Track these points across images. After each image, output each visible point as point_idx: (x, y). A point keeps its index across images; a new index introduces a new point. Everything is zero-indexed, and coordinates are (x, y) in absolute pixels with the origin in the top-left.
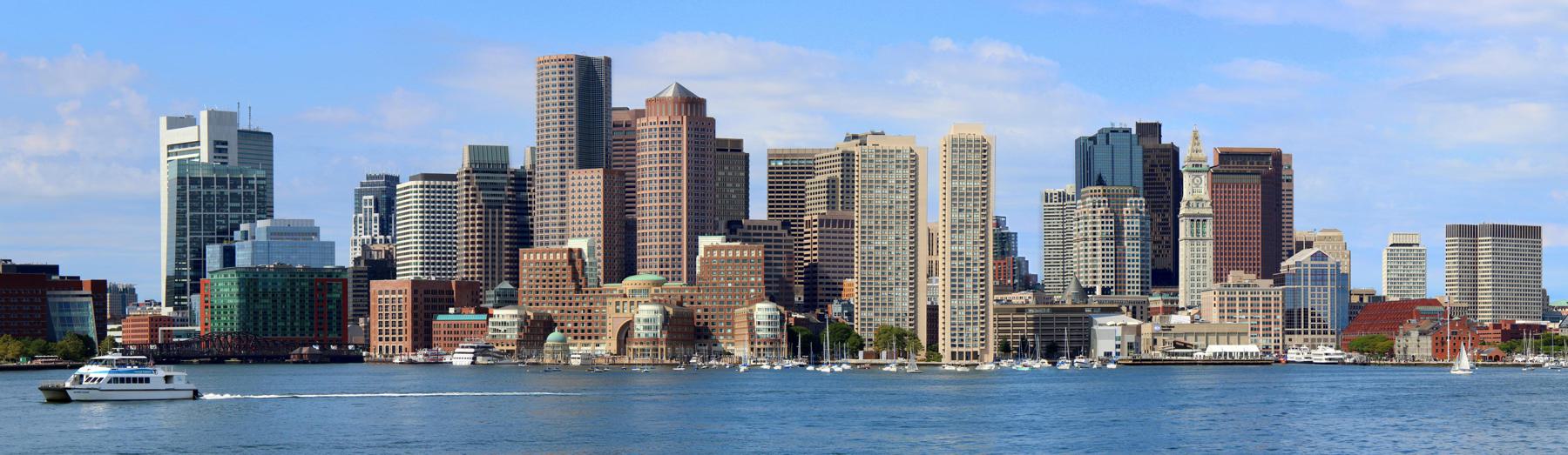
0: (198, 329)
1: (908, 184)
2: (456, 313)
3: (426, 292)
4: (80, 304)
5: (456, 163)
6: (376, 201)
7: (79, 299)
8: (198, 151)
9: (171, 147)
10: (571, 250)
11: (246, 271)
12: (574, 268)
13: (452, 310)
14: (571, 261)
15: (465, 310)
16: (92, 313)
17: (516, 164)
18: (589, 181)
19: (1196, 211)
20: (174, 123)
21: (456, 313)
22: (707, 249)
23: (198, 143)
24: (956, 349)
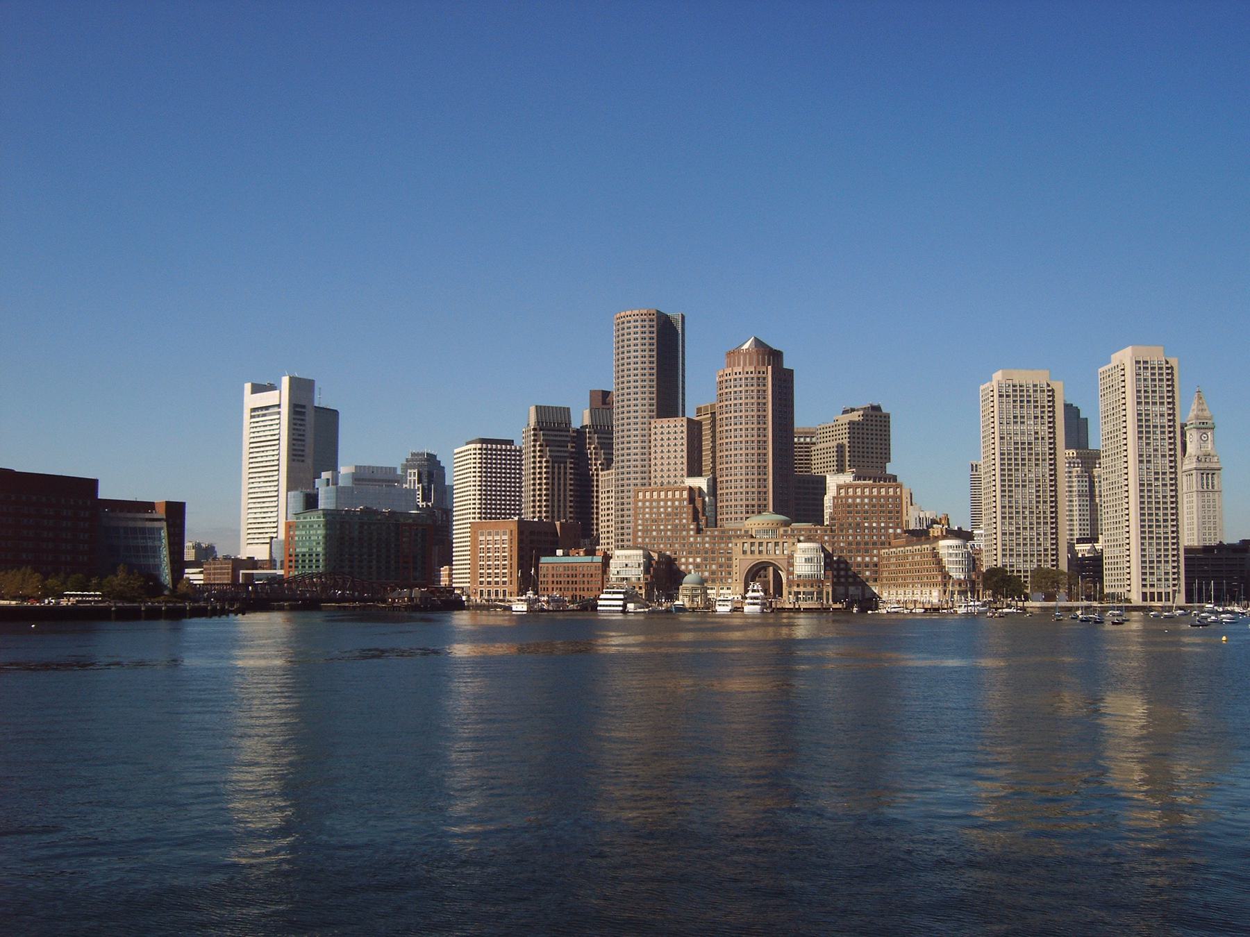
0: (280, 572)
1: (1046, 420)
2: (564, 555)
3: (532, 533)
4: (152, 530)
5: (519, 428)
6: (420, 474)
7: (149, 524)
8: (279, 413)
9: (254, 410)
10: (691, 489)
11: (327, 513)
12: (695, 509)
13: (559, 552)
14: (692, 500)
15: (572, 551)
16: (165, 542)
17: (576, 425)
18: (672, 430)
19: (1206, 465)
20: (257, 389)
21: (564, 555)
22: (839, 487)
23: (279, 406)
24: (1148, 590)
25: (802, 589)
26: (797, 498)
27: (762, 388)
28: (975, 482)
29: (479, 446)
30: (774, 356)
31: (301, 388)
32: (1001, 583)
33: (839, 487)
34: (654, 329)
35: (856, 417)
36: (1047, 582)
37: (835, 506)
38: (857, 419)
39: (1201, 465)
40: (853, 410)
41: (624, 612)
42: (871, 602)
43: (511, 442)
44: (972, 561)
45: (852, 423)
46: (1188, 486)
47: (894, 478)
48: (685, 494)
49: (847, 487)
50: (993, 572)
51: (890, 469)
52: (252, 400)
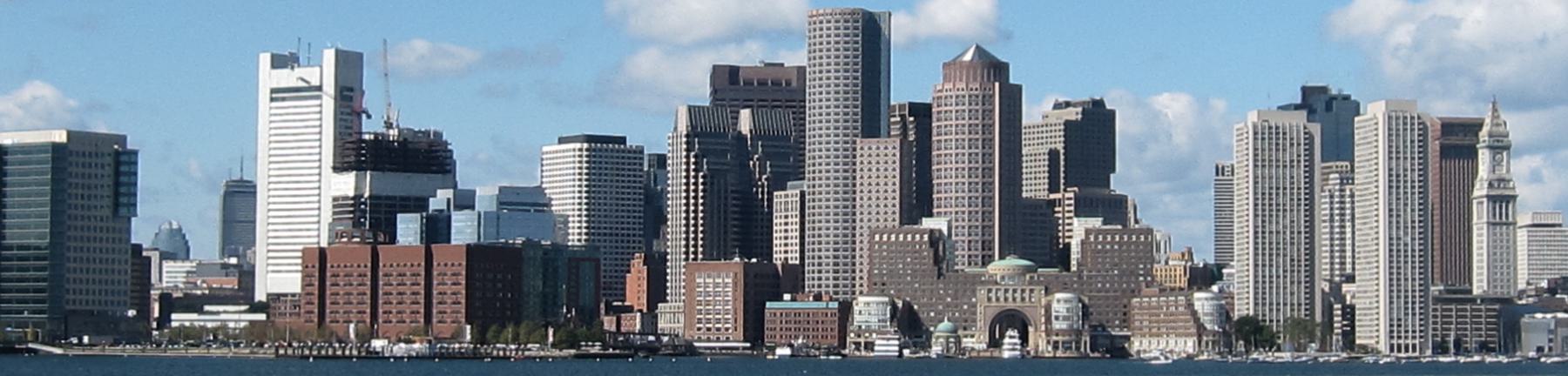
2: (793, 300)
9: (273, 91)
13: (787, 297)
19: (1499, 192)
20: (278, 62)
21: (793, 300)
25: (1060, 338)
26: (1030, 233)
27: (987, 107)
28: (1224, 193)
29: (586, 145)
30: (997, 69)
31: (349, 64)
32: (1254, 332)
33: (1088, 232)
34: (859, 32)
35: (1074, 114)
36: (1302, 330)
37: (1083, 251)
38: (1073, 118)
39: (1493, 193)
40: (1068, 104)
41: (901, 355)
42: (1123, 353)
43: (622, 140)
44: (1224, 314)
45: (1067, 124)
46: (1480, 216)
47: (1121, 201)
48: (926, 237)
49: (1098, 232)
50: (1245, 320)
51: (1117, 184)
52: (271, 78)
